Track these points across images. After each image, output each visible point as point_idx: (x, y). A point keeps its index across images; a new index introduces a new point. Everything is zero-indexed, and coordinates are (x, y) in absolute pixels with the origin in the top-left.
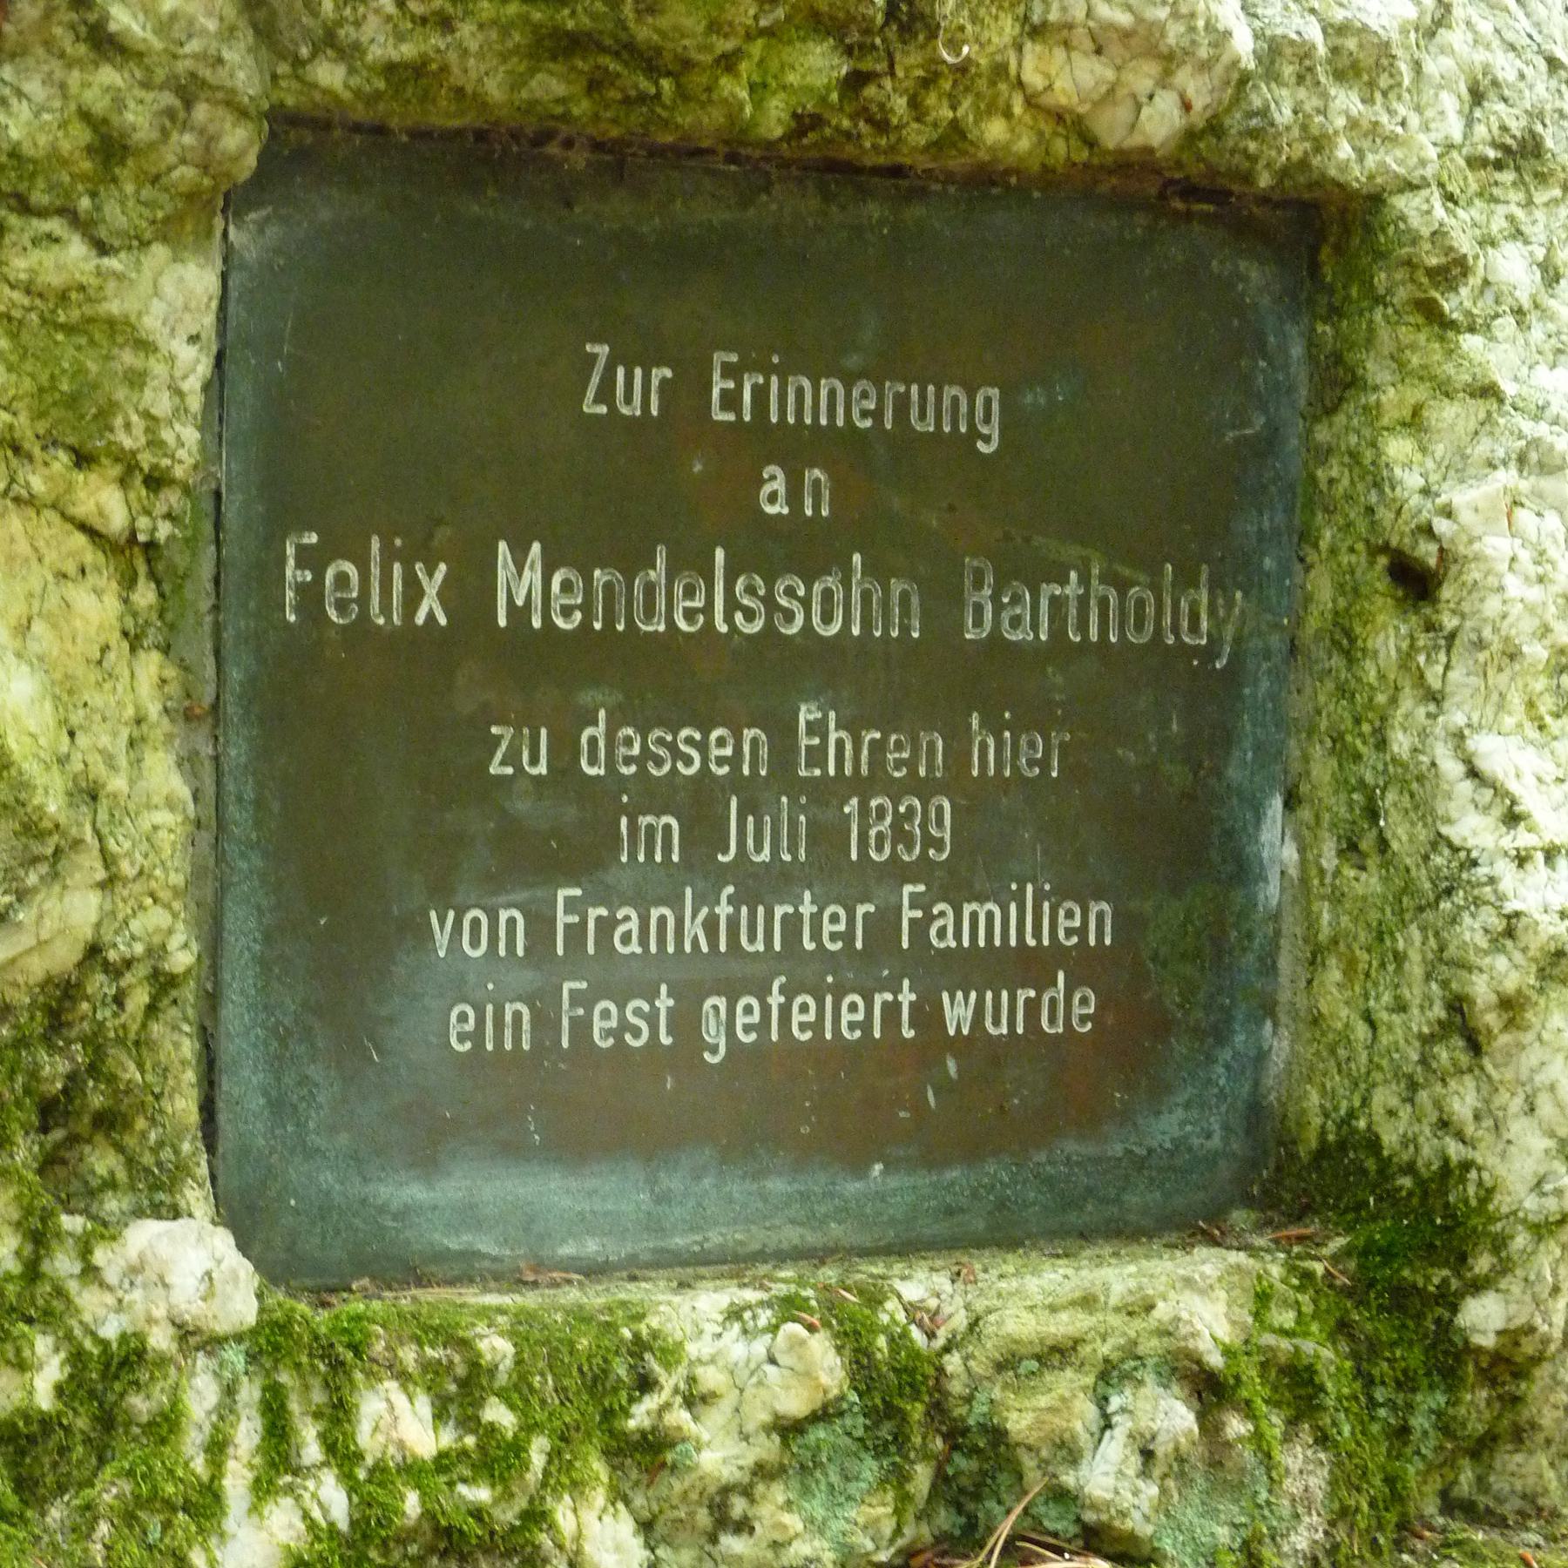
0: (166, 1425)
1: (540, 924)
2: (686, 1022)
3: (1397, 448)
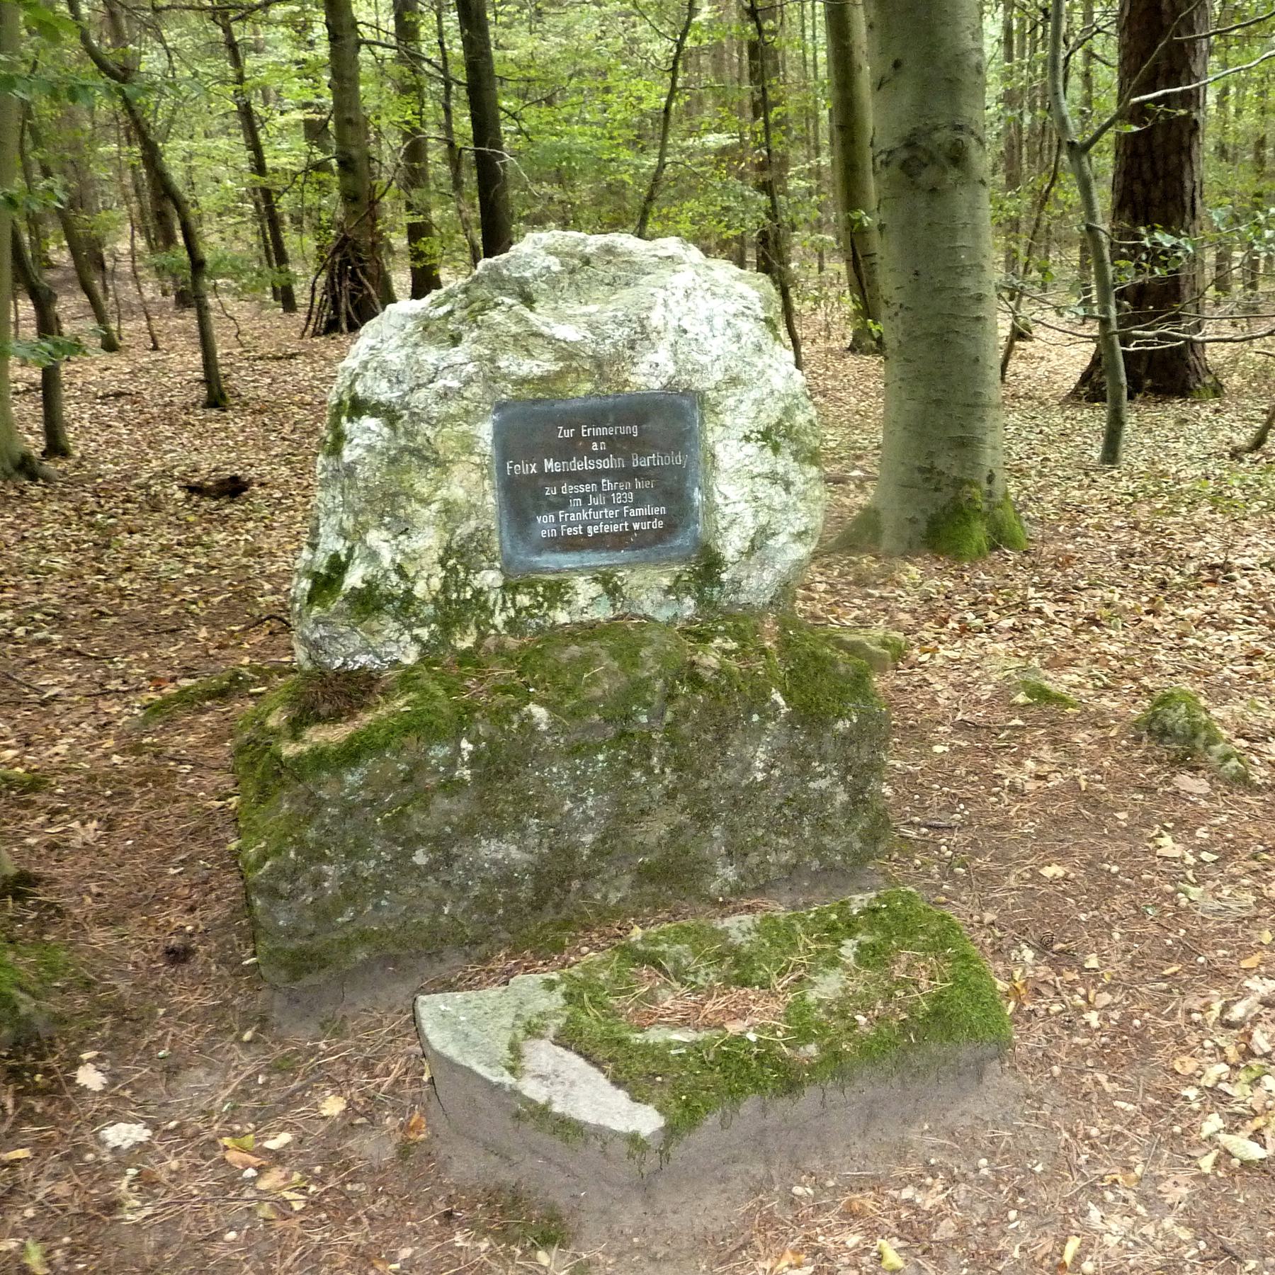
0: (486, 601)
1: (557, 518)
2: (584, 530)
3: (709, 434)
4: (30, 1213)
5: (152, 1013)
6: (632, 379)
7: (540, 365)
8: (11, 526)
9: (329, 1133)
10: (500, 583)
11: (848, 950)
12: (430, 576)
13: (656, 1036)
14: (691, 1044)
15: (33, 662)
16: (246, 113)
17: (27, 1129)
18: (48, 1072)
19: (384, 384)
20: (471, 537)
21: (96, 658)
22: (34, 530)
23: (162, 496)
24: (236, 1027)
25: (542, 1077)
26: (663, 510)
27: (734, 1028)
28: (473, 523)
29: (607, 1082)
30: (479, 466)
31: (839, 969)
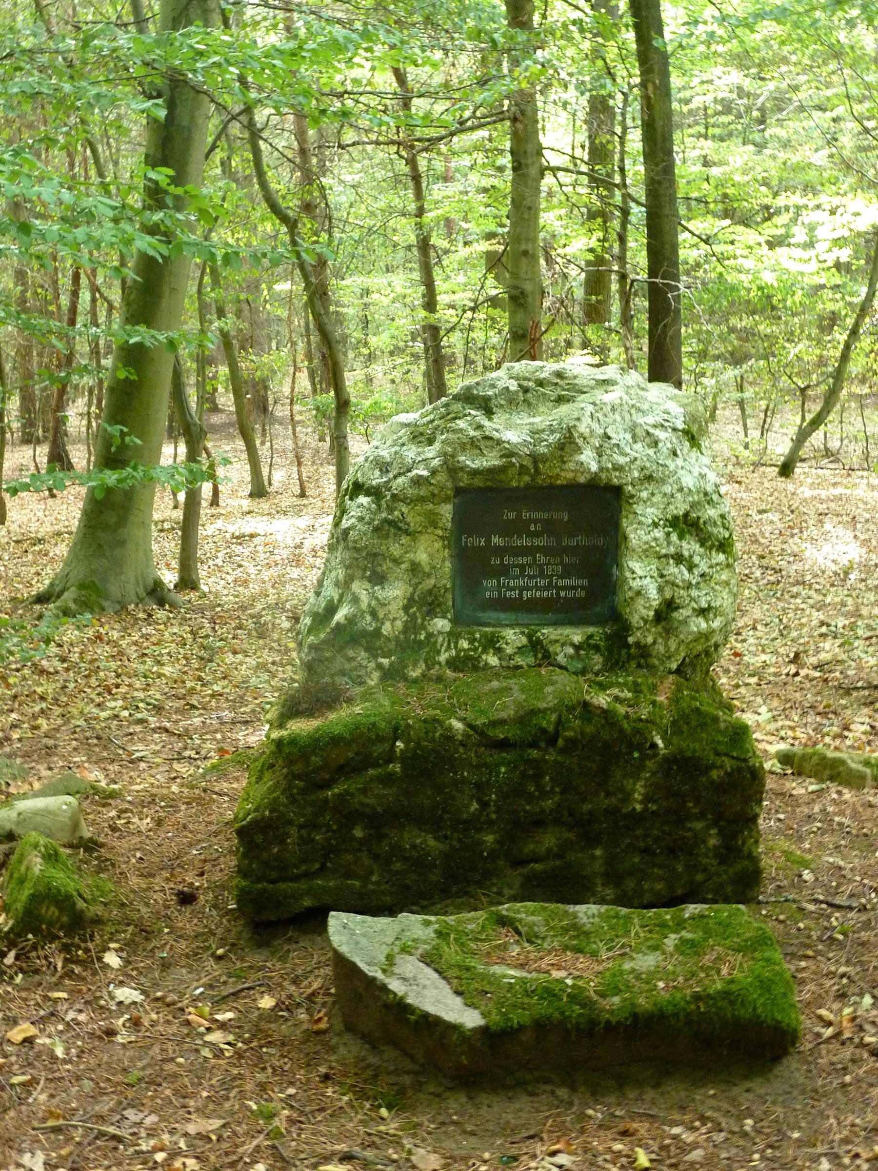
0: (436, 642)
1: (499, 582)
2: (521, 594)
4: (60, 1027)
5: (160, 931)
6: (563, 474)
7: (490, 460)
8: (135, 643)
9: (260, 1017)
10: (448, 629)
11: (671, 941)
12: (395, 619)
13: (497, 969)
14: (521, 978)
15: (131, 734)
16: (424, 245)
17: (67, 982)
18: (87, 950)
19: (377, 473)
20: (430, 592)
21: (179, 735)
22: (154, 648)
23: (270, 626)
24: (214, 946)
25: (405, 979)
26: (585, 582)
27: (556, 974)
28: (432, 581)
29: (450, 991)
30: (442, 538)
31: (658, 953)
